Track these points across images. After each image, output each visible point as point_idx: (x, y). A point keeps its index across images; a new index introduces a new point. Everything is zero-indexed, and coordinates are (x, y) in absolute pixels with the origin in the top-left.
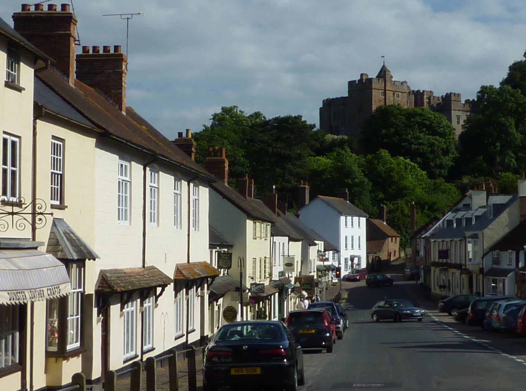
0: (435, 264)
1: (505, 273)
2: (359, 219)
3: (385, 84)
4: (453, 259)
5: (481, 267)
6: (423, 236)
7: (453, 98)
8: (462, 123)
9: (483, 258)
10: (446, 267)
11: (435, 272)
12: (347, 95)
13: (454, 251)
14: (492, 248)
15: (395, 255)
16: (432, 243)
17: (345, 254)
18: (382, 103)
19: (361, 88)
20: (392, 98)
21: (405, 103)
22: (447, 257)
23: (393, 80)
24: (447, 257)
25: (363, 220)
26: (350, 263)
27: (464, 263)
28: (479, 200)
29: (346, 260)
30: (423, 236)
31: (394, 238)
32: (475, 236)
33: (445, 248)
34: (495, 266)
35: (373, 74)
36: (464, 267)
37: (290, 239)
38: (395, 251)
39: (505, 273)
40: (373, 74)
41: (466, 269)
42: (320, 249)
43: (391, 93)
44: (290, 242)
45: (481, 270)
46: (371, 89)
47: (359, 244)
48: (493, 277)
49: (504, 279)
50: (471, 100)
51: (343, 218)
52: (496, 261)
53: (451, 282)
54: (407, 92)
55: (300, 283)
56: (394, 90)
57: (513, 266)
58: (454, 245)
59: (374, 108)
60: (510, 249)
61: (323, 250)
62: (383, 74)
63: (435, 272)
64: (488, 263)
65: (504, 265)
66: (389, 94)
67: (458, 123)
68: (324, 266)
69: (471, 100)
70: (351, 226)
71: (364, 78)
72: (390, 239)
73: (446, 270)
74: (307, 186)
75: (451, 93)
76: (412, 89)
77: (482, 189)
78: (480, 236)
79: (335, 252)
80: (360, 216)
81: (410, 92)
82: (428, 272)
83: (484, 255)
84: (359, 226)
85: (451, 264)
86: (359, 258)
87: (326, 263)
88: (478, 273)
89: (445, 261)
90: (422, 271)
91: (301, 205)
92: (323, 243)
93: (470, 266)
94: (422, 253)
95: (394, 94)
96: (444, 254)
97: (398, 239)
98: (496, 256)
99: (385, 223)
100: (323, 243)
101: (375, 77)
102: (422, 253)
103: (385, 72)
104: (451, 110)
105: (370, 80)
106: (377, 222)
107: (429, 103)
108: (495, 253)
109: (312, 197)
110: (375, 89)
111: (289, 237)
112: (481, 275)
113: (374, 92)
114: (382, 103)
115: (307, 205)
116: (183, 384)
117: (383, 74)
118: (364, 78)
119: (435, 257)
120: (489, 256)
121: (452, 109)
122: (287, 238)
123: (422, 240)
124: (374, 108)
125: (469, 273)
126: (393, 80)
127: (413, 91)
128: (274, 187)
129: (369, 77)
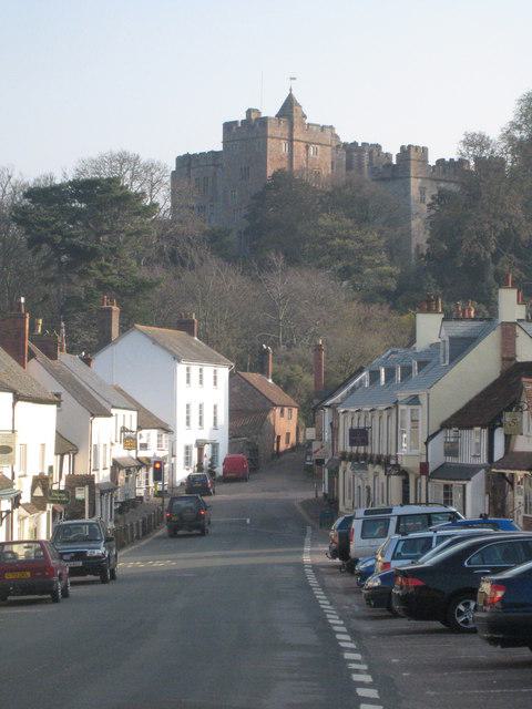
0: (344, 457)
1: (466, 472)
2: (201, 370)
3: (291, 130)
4: (377, 447)
5: (424, 460)
6: (328, 403)
7: (413, 155)
8: (429, 200)
9: (426, 444)
10: (361, 461)
11: (346, 469)
12: (219, 148)
13: (377, 425)
14: (445, 425)
15: (287, 442)
16: (342, 417)
17: (186, 436)
18: (284, 164)
19: (246, 134)
20: (303, 155)
21: (320, 162)
22: (365, 442)
23: (307, 121)
24: (365, 442)
25: (224, 373)
26: (195, 452)
27: (393, 454)
28: (430, 328)
29: (187, 448)
30: (328, 403)
31: (286, 409)
32: (415, 400)
33: (362, 426)
34: (450, 459)
35: (270, 110)
36: (393, 462)
37: (17, 398)
38: (288, 434)
39: (466, 472)
40: (270, 110)
41: (397, 466)
42: (127, 426)
43: (302, 145)
44: (19, 403)
45: (424, 467)
46: (266, 137)
47: (188, 418)
48: (445, 482)
49: (464, 486)
50: (447, 160)
51: (181, 368)
52: (452, 450)
53: (372, 492)
54: (334, 145)
55: (44, 489)
56: (307, 139)
57: (483, 460)
58: (377, 418)
59: (270, 172)
60: (477, 426)
61: (134, 428)
62: (289, 109)
63: (346, 469)
64: (436, 456)
65: (466, 458)
66: (299, 147)
67: (423, 200)
68: (138, 459)
69: (447, 160)
70: (198, 383)
71: (253, 116)
72: (278, 410)
73: (364, 467)
74: (115, 308)
75: (409, 146)
76: (343, 140)
77: (436, 312)
78: (423, 399)
79: (162, 432)
80: (217, 362)
81: (338, 146)
82: (334, 473)
83: (430, 438)
84: (215, 384)
85: (372, 456)
86: (215, 446)
87: (142, 454)
88: (418, 472)
89: (361, 450)
90: (326, 470)
91: (105, 341)
92: (135, 414)
93: (404, 463)
94: (327, 436)
95: (307, 148)
96: (359, 436)
97: (295, 411)
98: (452, 440)
99: (270, 381)
100: (135, 414)
101: (274, 116)
102: (327, 436)
103: (291, 107)
104: (409, 177)
105: (263, 121)
106: (254, 378)
107: (370, 164)
108: (451, 433)
109: (125, 328)
110: (273, 138)
111: (15, 393)
112: (424, 477)
113: (271, 144)
114: (284, 164)
115: (115, 343)
116: (523, 653)
117: (289, 109)
118: (253, 116)
119: (344, 445)
120: (439, 439)
121: (412, 174)
122: (10, 395)
123: (327, 410)
124: (270, 172)
125: (404, 473)
126: (307, 121)
127: (345, 145)
128: (23, 300)
129: (263, 115)
